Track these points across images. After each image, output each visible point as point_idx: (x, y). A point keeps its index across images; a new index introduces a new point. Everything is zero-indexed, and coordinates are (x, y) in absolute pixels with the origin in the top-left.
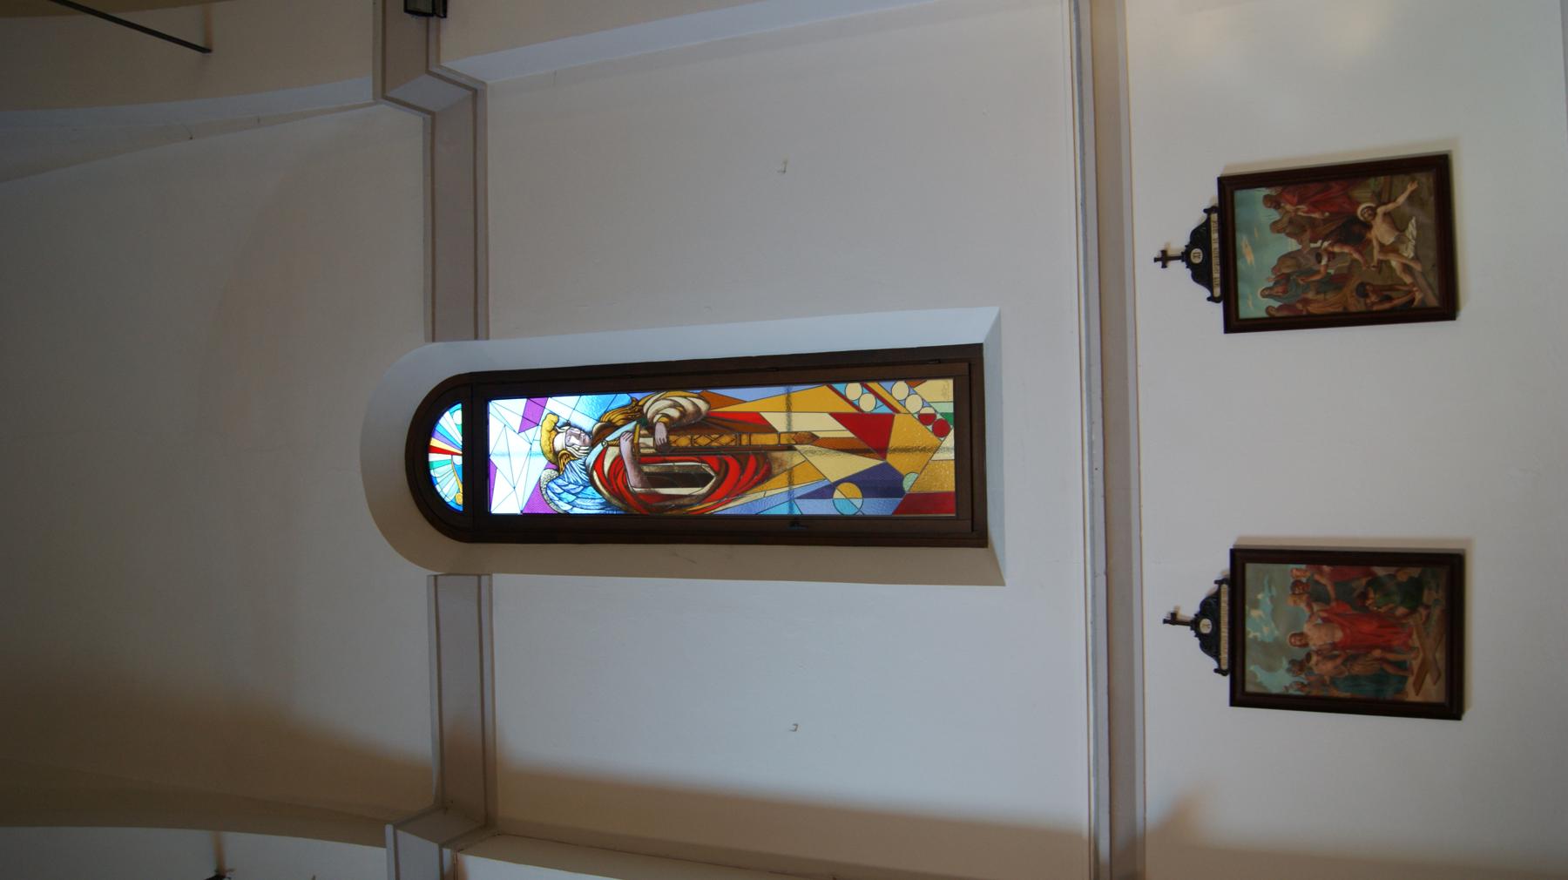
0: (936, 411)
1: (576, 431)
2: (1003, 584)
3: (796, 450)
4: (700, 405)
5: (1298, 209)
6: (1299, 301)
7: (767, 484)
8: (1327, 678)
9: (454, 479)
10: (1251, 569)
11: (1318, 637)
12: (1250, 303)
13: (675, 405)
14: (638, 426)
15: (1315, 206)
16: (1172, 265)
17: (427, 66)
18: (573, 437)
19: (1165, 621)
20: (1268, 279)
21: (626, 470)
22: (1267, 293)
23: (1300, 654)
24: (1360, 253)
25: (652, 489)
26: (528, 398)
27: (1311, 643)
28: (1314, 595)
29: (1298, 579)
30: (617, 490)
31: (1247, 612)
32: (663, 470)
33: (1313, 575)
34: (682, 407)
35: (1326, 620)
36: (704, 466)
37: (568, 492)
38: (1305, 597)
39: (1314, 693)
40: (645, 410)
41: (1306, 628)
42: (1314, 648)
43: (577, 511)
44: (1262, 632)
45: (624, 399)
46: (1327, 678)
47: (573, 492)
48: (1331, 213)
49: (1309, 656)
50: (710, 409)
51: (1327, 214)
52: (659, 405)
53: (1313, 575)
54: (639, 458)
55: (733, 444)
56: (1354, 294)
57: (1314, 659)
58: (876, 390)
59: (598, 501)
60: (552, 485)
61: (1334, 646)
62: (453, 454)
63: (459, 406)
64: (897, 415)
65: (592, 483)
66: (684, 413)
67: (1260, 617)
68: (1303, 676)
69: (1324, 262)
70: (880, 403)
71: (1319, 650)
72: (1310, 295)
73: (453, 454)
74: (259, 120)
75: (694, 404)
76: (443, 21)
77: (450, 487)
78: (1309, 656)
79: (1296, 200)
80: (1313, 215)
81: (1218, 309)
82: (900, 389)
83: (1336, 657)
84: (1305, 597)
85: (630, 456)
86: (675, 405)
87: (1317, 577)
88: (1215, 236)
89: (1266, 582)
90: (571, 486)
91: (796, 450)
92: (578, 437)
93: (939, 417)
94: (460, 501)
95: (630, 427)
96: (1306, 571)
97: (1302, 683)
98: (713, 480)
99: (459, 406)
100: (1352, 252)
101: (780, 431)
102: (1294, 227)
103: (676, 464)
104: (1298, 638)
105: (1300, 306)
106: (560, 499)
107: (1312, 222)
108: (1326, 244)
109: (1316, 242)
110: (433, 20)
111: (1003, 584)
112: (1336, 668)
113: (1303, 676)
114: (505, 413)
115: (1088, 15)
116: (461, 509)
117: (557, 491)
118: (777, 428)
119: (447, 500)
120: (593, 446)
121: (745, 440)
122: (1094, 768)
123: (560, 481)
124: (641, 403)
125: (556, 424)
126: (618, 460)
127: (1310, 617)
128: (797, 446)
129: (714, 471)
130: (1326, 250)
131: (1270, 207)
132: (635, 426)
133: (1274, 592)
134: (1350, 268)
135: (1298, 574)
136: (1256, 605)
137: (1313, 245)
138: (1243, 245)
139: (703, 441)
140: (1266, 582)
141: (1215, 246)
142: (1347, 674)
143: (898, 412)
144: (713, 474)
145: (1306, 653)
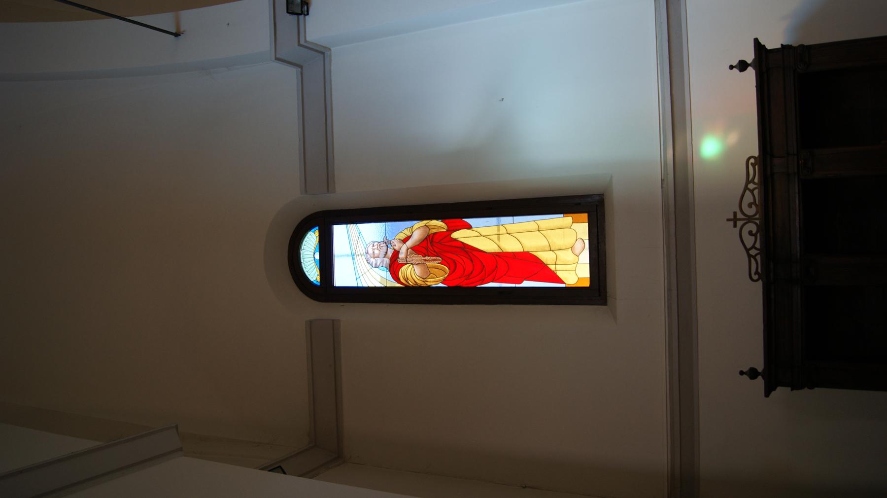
9: (316, 269)
17: (299, 41)
19: (756, 41)
26: (590, 278)
63: (317, 228)
76: (307, 17)
77: (313, 273)
94: (319, 280)
99: (317, 228)
110: (301, 17)
114: (340, 232)
116: (319, 284)
119: (312, 280)
122: (662, 98)
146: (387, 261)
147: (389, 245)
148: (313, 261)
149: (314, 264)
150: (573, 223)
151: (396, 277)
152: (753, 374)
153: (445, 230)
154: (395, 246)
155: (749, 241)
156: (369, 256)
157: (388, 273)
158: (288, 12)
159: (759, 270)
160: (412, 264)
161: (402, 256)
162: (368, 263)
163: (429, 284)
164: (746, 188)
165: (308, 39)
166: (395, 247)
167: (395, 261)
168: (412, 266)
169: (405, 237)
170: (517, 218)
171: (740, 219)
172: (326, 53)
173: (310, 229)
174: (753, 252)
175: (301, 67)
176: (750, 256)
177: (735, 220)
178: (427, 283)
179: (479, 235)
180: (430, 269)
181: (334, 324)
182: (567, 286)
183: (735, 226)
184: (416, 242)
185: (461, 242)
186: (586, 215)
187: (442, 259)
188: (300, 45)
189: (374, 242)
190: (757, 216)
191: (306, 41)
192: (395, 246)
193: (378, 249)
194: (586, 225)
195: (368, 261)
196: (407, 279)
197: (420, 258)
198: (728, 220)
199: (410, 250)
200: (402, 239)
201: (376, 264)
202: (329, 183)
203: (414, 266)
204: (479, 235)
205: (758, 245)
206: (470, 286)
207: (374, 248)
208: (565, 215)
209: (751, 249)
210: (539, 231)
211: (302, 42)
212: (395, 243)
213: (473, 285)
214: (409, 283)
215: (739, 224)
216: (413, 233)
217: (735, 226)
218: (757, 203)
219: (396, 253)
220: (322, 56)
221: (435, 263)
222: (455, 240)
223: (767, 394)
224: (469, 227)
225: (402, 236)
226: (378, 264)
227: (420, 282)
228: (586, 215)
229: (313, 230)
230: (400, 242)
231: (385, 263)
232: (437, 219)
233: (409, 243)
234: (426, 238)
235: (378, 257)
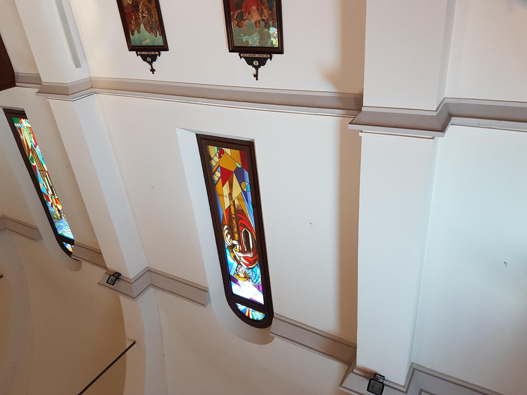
0: (217, 152)
1: (238, 268)
2: (254, 139)
3: (234, 201)
4: (226, 228)
5: (133, 24)
6: (156, 24)
7: (245, 212)
8: (270, 12)
10: (236, 44)
11: (256, 17)
12: (159, 41)
13: (227, 235)
14: (234, 249)
15: (132, 18)
16: (154, 68)
18: (240, 270)
20: (152, 34)
21: (247, 257)
22: (156, 36)
23: (262, 23)
24: (140, 2)
25: (251, 250)
27: (258, 19)
28: (241, 18)
29: (236, 25)
30: (253, 261)
31: (250, 46)
32: (245, 245)
33: (234, 19)
34: (227, 233)
35: (249, 14)
36: (243, 231)
37: (255, 277)
38: (242, 22)
39: (275, 17)
40: (230, 245)
41: (253, 22)
42: (260, 18)
43: (260, 276)
44: (256, 40)
45: (228, 252)
46: (270, 12)
47: (255, 276)
48: (132, 13)
49: (263, 20)
50: (226, 225)
51: (133, 14)
52: (228, 241)
53: (234, 19)
54: (242, 251)
55: (235, 220)
56: (151, 4)
57: (263, 18)
58: (215, 169)
59: (257, 268)
60: (254, 281)
61: (258, 9)
62: (249, 311)
64: (220, 165)
65: (252, 268)
66: (229, 233)
67: (251, 41)
68: (270, 22)
69: (145, 15)
70: (218, 170)
71: (260, 16)
72: (154, 20)
73: (249, 311)
74: (161, 334)
75: (226, 229)
78: (263, 20)
79: (131, 25)
80: (134, 19)
81: (274, 56)
82: (213, 163)
83: (261, 8)
84: (242, 22)
85: (243, 254)
86: (227, 235)
87: (235, 17)
88: (143, 53)
89: (239, 38)
90: (254, 275)
91: (234, 201)
92: (239, 269)
93: (219, 152)
95: (234, 251)
96: (234, 22)
97: (273, 23)
98: (246, 229)
100: (140, 5)
101: (229, 205)
102: (138, 25)
103: (243, 240)
104: (257, 25)
105: (157, 24)
106: (258, 280)
107: (136, 19)
108: (140, 14)
109: (140, 18)
111: (254, 139)
112: (265, 9)
113: (270, 22)
115: (98, 89)
117: (256, 281)
118: (229, 205)
120: (241, 265)
121: (234, 216)
123: (253, 279)
124: (228, 246)
125: (237, 274)
126: (244, 258)
127: (249, 20)
128: (233, 200)
129: (243, 229)
130: (141, 15)
131: (134, 33)
132: (234, 250)
133: (242, 35)
134: (145, 6)
135: (235, 25)
136: (248, 42)
137: (141, 19)
138: (145, 43)
139: (236, 230)
140: (239, 38)
141: (146, 53)
142: (267, 4)
143: (219, 165)
144: (244, 229)
145: (262, 21)
165: (403, 385)
172: (414, 367)
191: (404, 387)
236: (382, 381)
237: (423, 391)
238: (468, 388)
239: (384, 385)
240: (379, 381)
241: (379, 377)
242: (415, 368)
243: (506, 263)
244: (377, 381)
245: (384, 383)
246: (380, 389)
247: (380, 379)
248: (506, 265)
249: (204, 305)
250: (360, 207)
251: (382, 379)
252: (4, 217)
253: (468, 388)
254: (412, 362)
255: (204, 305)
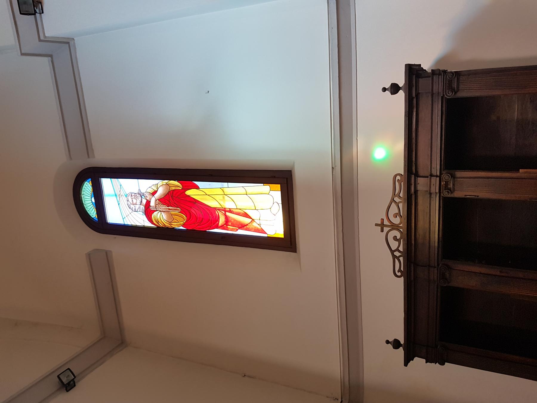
9: (94, 210)
63: (90, 179)
77: (93, 212)
99: (90, 179)
114: (106, 183)
119: (93, 217)
146: (142, 207)
147: (143, 197)
148: (92, 203)
149: (92, 205)
150: (270, 190)
151: (150, 220)
152: (396, 344)
153: (181, 189)
154: (147, 197)
155: (394, 245)
156: (129, 203)
157: (145, 216)
158: (21, 13)
159: (402, 269)
160: (160, 211)
161: (152, 204)
162: (130, 208)
163: (173, 226)
164: (393, 200)
165: (46, 35)
166: (147, 198)
167: (148, 208)
168: (160, 212)
169: (153, 192)
170: (231, 184)
171: (386, 226)
172: (70, 42)
173: (85, 180)
174: (397, 254)
175: (51, 56)
176: (394, 257)
177: (382, 226)
178: (172, 225)
179: (205, 194)
180: (173, 216)
181: (107, 255)
182: (269, 236)
183: (382, 231)
184: (161, 196)
185: (193, 198)
186: (279, 185)
187: (181, 209)
188: (40, 40)
189: (132, 193)
190: (401, 225)
191: (45, 37)
192: (147, 197)
193: (135, 199)
194: (279, 193)
195: (130, 207)
196: (158, 222)
197: (164, 207)
198: (377, 225)
199: (157, 200)
200: (151, 192)
201: (135, 209)
202: (88, 149)
203: (162, 213)
204: (205, 194)
205: (401, 249)
206: (201, 230)
207: (132, 197)
208: (264, 184)
209: (395, 251)
210: (246, 194)
211: (42, 38)
212: (147, 195)
213: (204, 230)
214: (159, 225)
215: (386, 229)
216: (158, 189)
217: (382, 231)
218: (401, 214)
219: (148, 202)
220: (68, 45)
221: (176, 211)
222: (188, 196)
223: (406, 364)
224: (197, 187)
225: (151, 191)
226: (137, 209)
227: (167, 225)
228: (279, 185)
229: (88, 181)
230: (150, 195)
231: (141, 209)
232: (175, 180)
233: (157, 195)
234: (168, 193)
235: (136, 204)
236: (37, 11)
237: (52, 58)
238: (82, 117)
239: (34, 14)
240: (36, 9)
241: (39, 7)
242: (70, 43)
243: (208, 93)
244: (34, 6)
245: (37, 14)
246: (27, 11)
247: (38, 8)
248: (207, 93)
249: (106, 253)
250: (415, 64)
251: (40, 10)
252: (41, 3)
253: (82, 117)
254: (75, 38)
255: (106, 253)
